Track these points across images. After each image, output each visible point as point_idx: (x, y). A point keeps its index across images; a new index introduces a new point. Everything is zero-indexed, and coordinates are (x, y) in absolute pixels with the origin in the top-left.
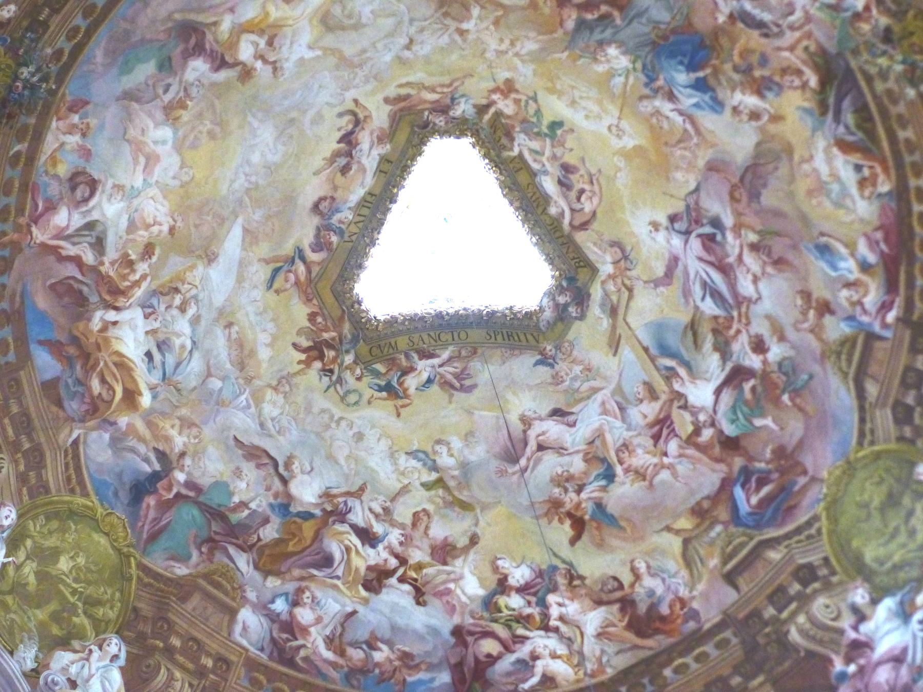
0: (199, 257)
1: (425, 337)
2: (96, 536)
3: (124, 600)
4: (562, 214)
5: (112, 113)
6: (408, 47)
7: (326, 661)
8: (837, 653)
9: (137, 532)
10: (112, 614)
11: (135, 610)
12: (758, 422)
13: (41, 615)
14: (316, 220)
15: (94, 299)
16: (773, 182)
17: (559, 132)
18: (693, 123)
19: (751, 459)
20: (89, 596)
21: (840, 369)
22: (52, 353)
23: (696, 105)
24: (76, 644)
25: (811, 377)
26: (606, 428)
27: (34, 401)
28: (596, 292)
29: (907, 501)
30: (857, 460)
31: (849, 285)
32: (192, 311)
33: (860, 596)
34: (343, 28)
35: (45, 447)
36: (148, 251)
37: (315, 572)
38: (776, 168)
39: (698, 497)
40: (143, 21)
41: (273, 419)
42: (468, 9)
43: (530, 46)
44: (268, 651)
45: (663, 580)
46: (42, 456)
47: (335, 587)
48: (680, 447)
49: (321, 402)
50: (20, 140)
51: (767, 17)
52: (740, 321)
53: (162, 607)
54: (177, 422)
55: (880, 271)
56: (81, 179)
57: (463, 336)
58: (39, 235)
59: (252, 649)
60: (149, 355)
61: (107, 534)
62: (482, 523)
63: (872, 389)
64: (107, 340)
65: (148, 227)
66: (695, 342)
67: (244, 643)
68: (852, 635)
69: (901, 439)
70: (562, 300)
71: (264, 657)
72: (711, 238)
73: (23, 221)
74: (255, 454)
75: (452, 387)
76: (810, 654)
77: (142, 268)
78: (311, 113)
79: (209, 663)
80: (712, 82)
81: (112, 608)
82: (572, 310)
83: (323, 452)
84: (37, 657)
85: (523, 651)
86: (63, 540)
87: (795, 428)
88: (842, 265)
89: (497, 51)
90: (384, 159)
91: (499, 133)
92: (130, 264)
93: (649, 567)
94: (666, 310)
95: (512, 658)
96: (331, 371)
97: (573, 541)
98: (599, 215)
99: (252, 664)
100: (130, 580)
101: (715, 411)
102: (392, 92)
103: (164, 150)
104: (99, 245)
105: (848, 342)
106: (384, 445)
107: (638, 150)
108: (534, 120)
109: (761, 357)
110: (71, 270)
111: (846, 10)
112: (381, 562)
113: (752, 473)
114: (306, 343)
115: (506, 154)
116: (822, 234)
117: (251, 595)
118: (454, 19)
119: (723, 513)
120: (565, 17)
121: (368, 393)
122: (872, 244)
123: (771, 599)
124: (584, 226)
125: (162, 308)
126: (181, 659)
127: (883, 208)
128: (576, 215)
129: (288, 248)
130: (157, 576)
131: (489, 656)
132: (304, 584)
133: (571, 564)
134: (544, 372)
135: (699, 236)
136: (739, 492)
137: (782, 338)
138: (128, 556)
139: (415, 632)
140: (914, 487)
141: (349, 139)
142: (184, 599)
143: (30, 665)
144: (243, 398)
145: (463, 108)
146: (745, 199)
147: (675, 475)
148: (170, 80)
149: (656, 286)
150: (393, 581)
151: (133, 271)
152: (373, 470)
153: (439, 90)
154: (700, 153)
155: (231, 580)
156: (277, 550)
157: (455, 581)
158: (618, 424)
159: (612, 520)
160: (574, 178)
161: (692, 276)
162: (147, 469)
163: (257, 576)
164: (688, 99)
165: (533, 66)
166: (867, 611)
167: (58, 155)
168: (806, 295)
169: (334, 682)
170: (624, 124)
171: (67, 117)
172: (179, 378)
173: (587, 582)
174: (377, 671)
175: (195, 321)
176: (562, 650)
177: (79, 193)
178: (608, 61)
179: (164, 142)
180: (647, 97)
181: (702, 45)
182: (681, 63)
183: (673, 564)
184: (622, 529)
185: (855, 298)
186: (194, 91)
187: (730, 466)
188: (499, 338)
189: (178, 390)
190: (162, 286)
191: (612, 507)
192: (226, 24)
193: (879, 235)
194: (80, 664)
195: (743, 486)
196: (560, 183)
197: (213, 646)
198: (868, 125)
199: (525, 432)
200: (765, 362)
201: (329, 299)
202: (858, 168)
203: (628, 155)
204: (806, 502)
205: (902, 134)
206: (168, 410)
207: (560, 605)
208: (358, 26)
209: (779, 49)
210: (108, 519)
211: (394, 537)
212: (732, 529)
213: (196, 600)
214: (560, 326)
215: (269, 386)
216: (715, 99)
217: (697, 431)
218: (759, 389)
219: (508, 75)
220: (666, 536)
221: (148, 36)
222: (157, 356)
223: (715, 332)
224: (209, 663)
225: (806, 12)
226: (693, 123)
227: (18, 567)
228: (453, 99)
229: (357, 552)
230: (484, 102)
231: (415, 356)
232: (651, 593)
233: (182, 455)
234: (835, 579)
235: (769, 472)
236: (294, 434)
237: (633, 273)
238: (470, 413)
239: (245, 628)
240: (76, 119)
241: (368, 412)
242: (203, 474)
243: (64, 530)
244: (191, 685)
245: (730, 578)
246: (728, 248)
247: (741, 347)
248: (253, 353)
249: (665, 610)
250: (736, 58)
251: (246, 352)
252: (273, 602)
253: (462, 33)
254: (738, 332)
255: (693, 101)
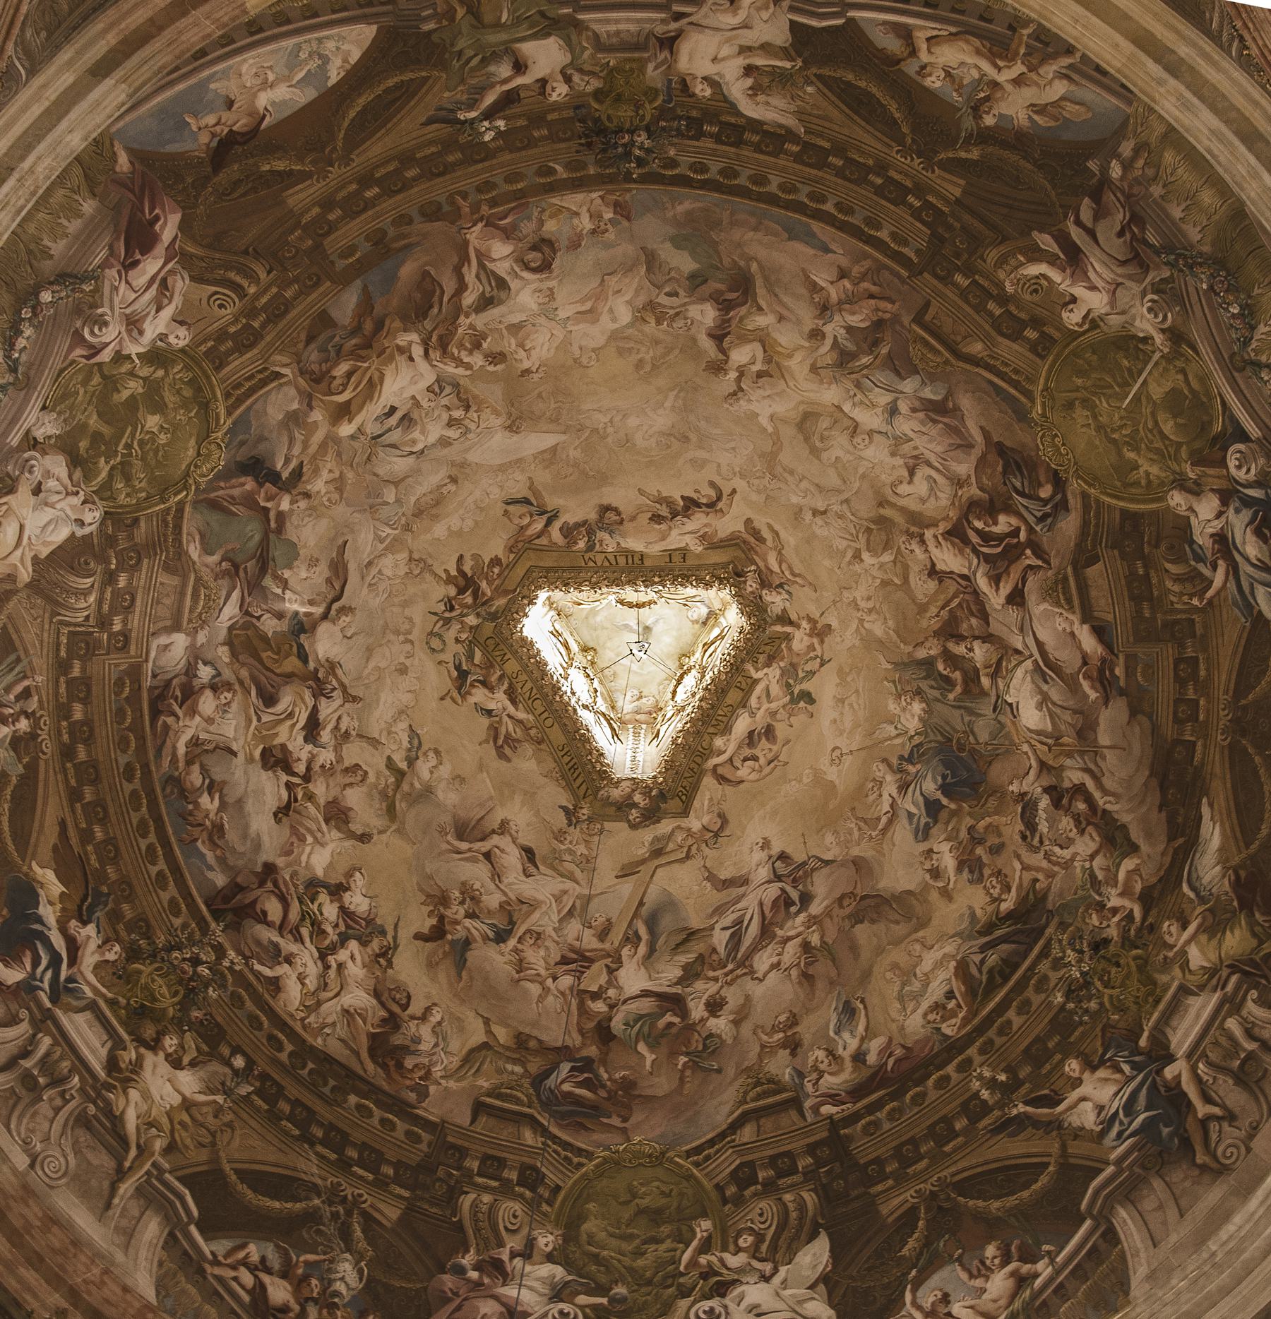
0: (509, 414)
1: (529, 685)
2: (192, 442)
3: (138, 507)
4: (721, 753)
5: (627, 249)
6: (816, 513)
7: (174, 748)
8: (478, 1252)
9: (212, 486)
10: (122, 499)
11: (136, 520)
12: (642, 1047)
13: (94, 422)
14: (593, 516)
15: (428, 324)
16: (880, 927)
17: (802, 704)
18: (890, 822)
19: (604, 1062)
20: (130, 464)
21: (746, 1093)
22: (358, 305)
23: (910, 815)
24: (78, 474)
25: (719, 1071)
26: (544, 908)
27: (301, 315)
28: (665, 826)
29: (665, 1229)
30: (671, 1161)
31: (831, 1053)
32: (452, 433)
33: (546, 1240)
34: (807, 439)
35: (263, 344)
36: (496, 357)
37: (253, 692)
38: (897, 922)
39: (535, 1033)
40: (737, 234)
41: (380, 572)
42: (885, 549)
43: (878, 629)
44: (156, 683)
45: (436, 1045)
46: (251, 346)
47: (250, 721)
48: (571, 988)
49: (417, 613)
50: (568, 166)
51: (1043, 827)
52: (726, 975)
53: (150, 548)
54: (337, 474)
55: (866, 1073)
56: (546, 250)
57: (549, 722)
58: (475, 236)
59: (150, 664)
60: (393, 410)
61: (199, 454)
62: (384, 837)
63: (747, 1133)
64: (391, 358)
65: (521, 345)
66: (678, 945)
67: (153, 654)
68: (505, 1257)
69: (719, 1188)
70: (638, 798)
71: (148, 682)
72: (789, 903)
73: (485, 210)
74: (339, 569)
75: (495, 739)
76: (459, 1227)
77: (477, 360)
78: (702, 454)
79: (117, 627)
80: (944, 815)
81: (128, 495)
82: (634, 814)
83: (371, 640)
84: (49, 437)
85: (288, 946)
86: (175, 409)
87: (662, 1085)
88: (846, 1035)
89: (855, 600)
90: (684, 552)
91: (767, 648)
92: (477, 346)
93: (439, 1023)
94: (692, 901)
95: (276, 938)
96: (452, 609)
97: (418, 936)
98: (742, 786)
99: (135, 672)
100: (163, 501)
101: (625, 1002)
102: (760, 523)
103: (606, 324)
104: (486, 303)
105: (776, 1086)
106: (406, 698)
107: (832, 786)
108: (801, 674)
109: (706, 1014)
110: (449, 286)
111: (1100, 895)
112: (295, 756)
113: (591, 1071)
114: (467, 568)
115: (749, 667)
116: (863, 1001)
117: (201, 638)
118: (868, 541)
119: (535, 1066)
120: (927, 644)
121: (448, 657)
122: (886, 1051)
123: (485, 1158)
124: (722, 779)
125: (445, 401)
126: (108, 595)
127: (927, 1039)
128: (728, 766)
129: (552, 502)
130: (178, 528)
131: (265, 913)
132: (237, 687)
133: (396, 947)
134: (560, 820)
135: (782, 890)
136: (565, 1068)
137: (736, 1023)
138: (186, 487)
139: (246, 827)
140: (684, 1228)
141: (691, 504)
142: (167, 568)
143: (39, 434)
144: (388, 531)
145: (776, 601)
146: (847, 911)
147: (541, 999)
148: (682, 293)
149: (707, 879)
150: (284, 778)
151: (471, 353)
152: (378, 701)
153: (784, 566)
154: (864, 844)
155: (207, 608)
156: (256, 642)
157: (315, 838)
158: (555, 918)
159: (461, 963)
160: (764, 743)
161: (739, 906)
162: (279, 466)
163: (223, 634)
164: (908, 804)
165: (857, 643)
166: (536, 1257)
167: (565, 214)
168: (794, 1021)
169: (159, 766)
170: (848, 760)
171: (607, 205)
172: (382, 454)
173: (390, 971)
174: (191, 807)
175: (444, 442)
176: (311, 983)
177: (531, 256)
178: (904, 710)
179: (614, 320)
180: (890, 766)
181: (974, 786)
182: (944, 777)
183: (458, 1046)
184: (460, 976)
185: (822, 1067)
186: (679, 323)
187: (584, 1045)
188: (566, 759)
189: (369, 459)
190: (466, 391)
191: (475, 956)
192: (762, 321)
193: (899, 1052)
194: (60, 488)
195: (572, 1069)
196: (751, 733)
197: (135, 623)
198: (998, 979)
199: (493, 832)
200: (702, 1020)
201: (520, 571)
202: (950, 995)
203: (818, 778)
204: (596, 1137)
205: (1011, 1014)
206: (344, 457)
207: (352, 957)
208: (815, 452)
209: (1018, 857)
210: (213, 447)
211: (326, 756)
212: (526, 1083)
213: (170, 581)
214: (611, 810)
215: (411, 552)
216: (927, 828)
217: (595, 996)
218: (674, 1030)
219: (835, 624)
220: (479, 1024)
221: (721, 247)
222: (393, 421)
223: (701, 958)
224: (117, 627)
225: (1073, 859)
226: (890, 822)
227: (132, 374)
228: (781, 585)
229: (293, 725)
230: (794, 617)
231: (506, 686)
232: (417, 1040)
233: (307, 495)
234: (545, 1207)
235: (604, 1086)
236: (375, 602)
237: (707, 851)
238: (481, 768)
239: (166, 647)
240: (608, 215)
241: (430, 666)
242: (297, 527)
243: (185, 405)
244: (87, 618)
245: (479, 1108)
246: (789, 924)
247: (703, 989)
248: (435, 518)
249: (409, 1062)
250: (982, 824)
251: (434, 511)
252: (205, 663)
253: (857, 556)
254: (716, 979)
255: (913, 810)
